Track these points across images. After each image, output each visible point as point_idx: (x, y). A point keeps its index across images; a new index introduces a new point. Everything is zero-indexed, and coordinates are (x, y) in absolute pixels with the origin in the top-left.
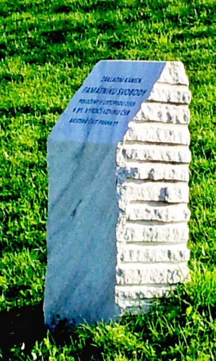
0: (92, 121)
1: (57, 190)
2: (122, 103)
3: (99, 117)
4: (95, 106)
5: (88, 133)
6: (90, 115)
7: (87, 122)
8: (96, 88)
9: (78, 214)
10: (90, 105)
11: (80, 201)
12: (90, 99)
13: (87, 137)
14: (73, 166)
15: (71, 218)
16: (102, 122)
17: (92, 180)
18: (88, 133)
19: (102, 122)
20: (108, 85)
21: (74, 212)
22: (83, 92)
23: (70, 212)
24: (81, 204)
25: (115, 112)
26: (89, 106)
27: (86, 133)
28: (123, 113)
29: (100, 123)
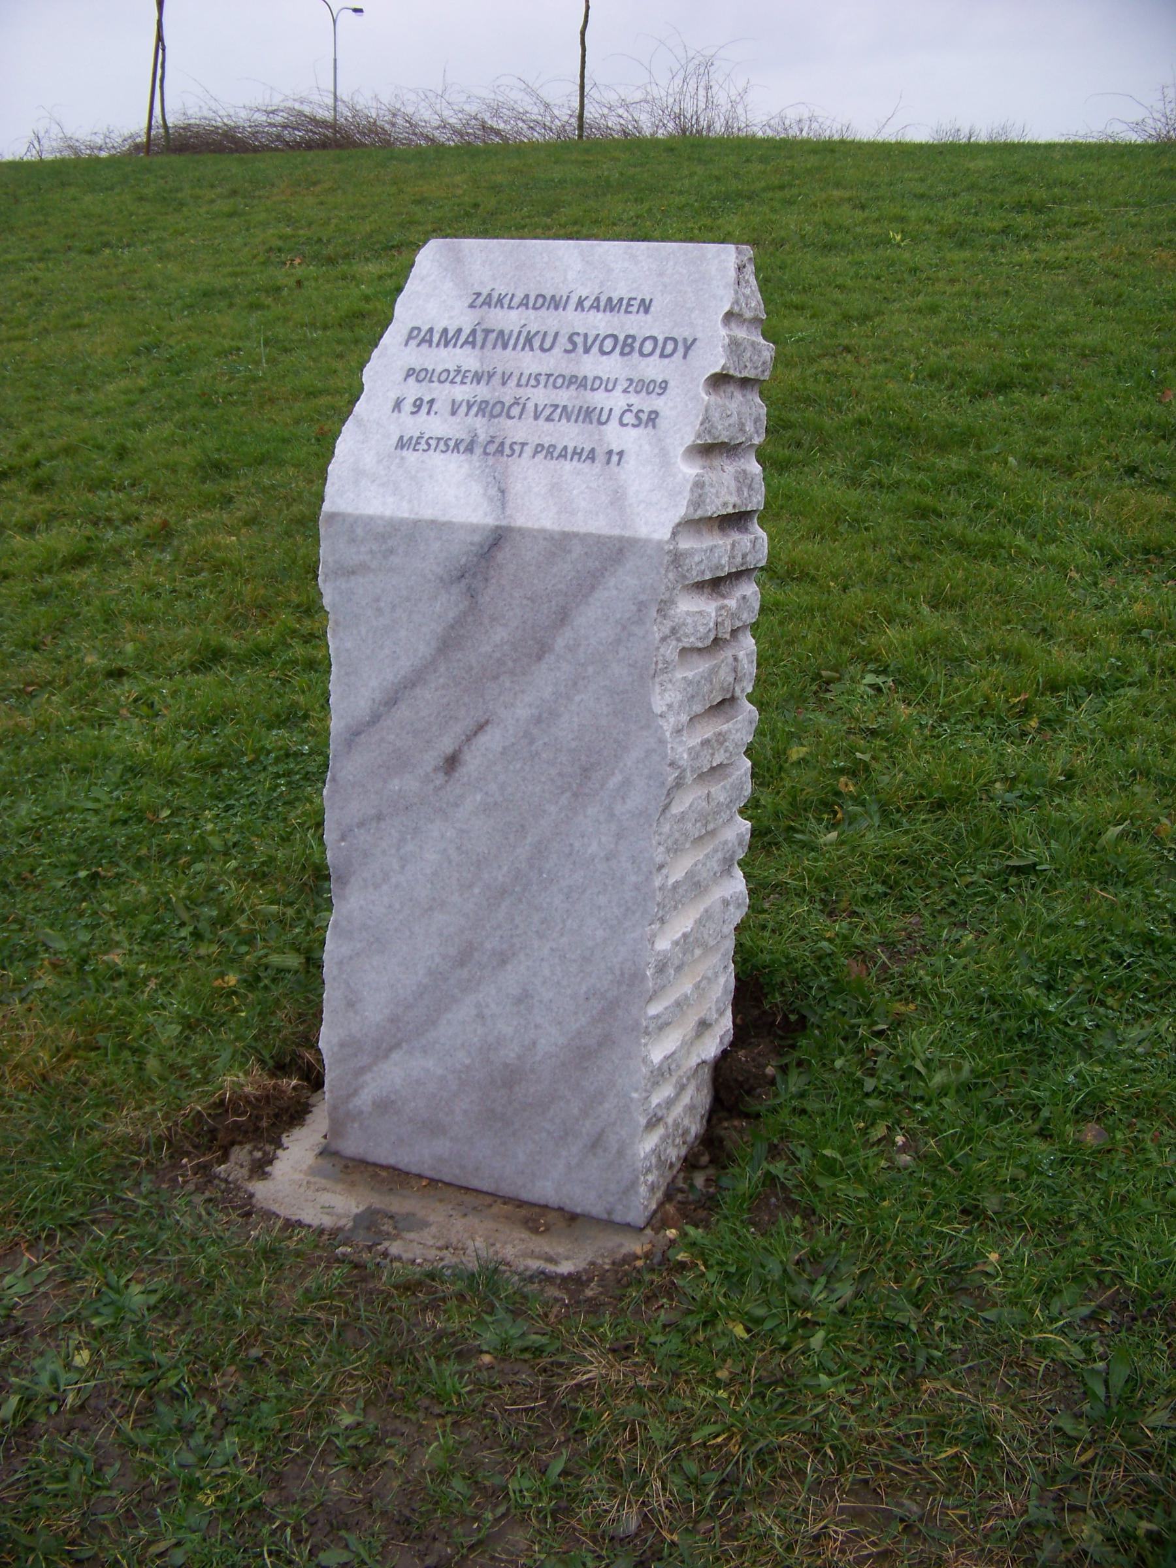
0: (499, 449)
1: (374, 683)
2: (609, 386)
3: (519, 430)
4: (482, 392)
5: (503, 492)
6: (481, 427)
7: (478, 451)
8: (459, 331)
9: (472, 763)
10: (466, 388)
11: (481, 727)
12: (452, 368)
13: (503, 506)
14: (447, 605)
15: (440, 778)
16: (548, 451)
17: (539, 658)
18: (503, 492)
19: (548, 451)
20: (510, 320)
21: (452, 762)
22: (695, 340)
23: (432, 759)
24: (483, 739)
25: (590, 415)
26: (461, 392)
27: (493, 491)
28: (629, 418)
29: (536, 452)
